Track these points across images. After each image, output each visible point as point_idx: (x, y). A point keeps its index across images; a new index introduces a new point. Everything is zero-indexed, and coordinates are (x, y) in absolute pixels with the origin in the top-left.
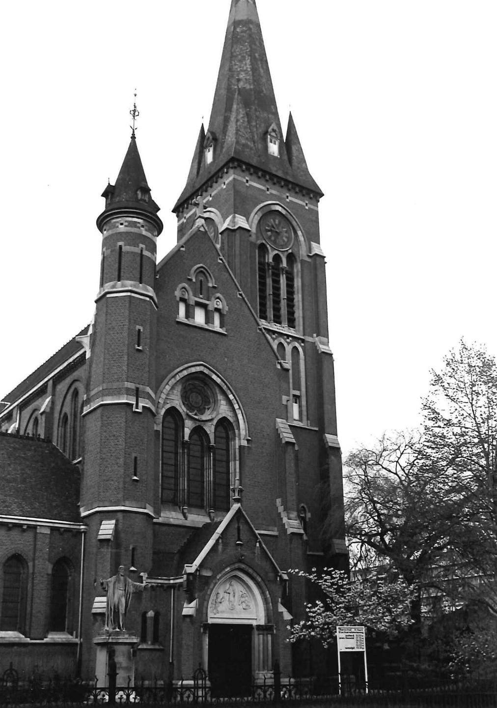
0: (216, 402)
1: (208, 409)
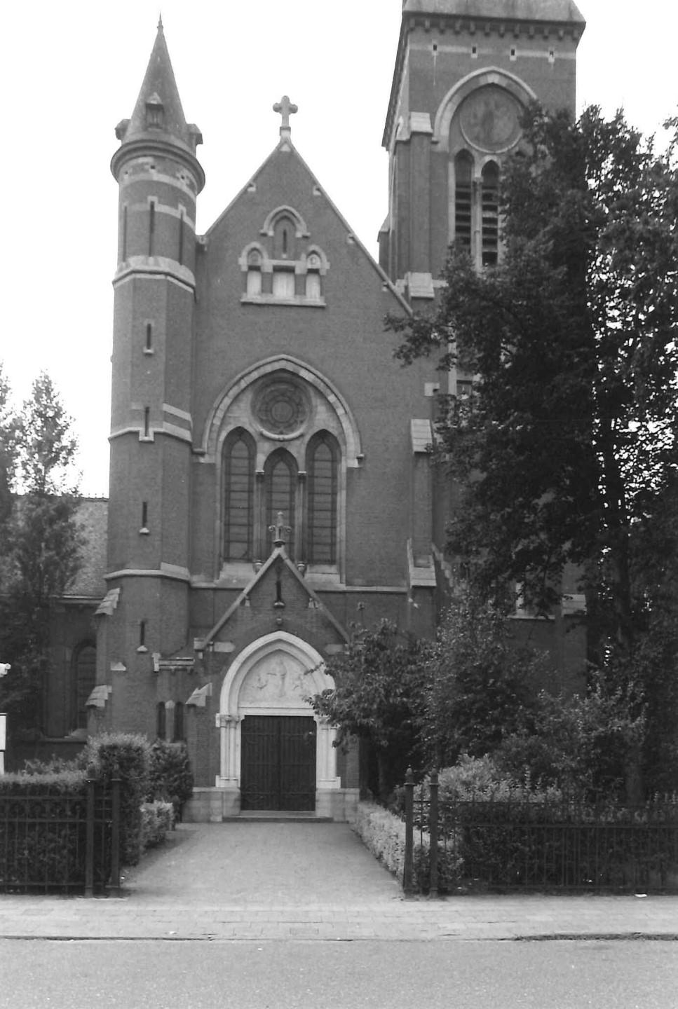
1: (302, 422)
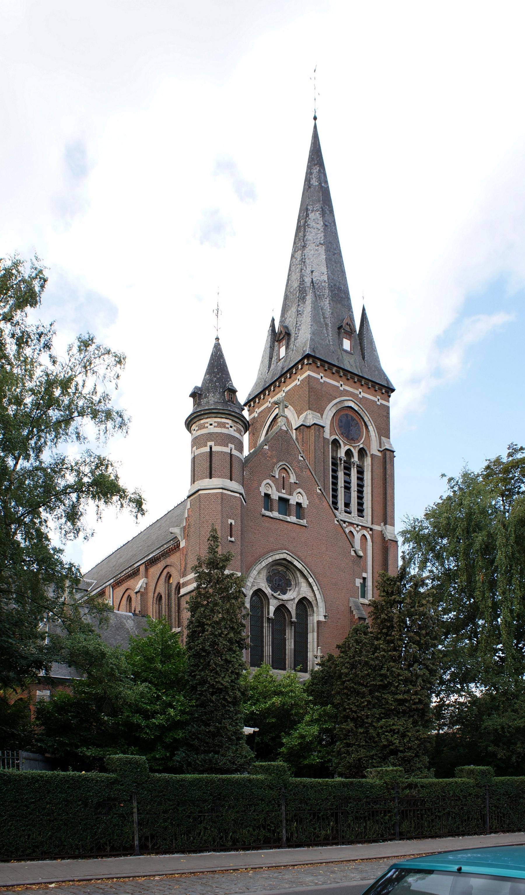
0: (297, 584)
1: (290, 590)
